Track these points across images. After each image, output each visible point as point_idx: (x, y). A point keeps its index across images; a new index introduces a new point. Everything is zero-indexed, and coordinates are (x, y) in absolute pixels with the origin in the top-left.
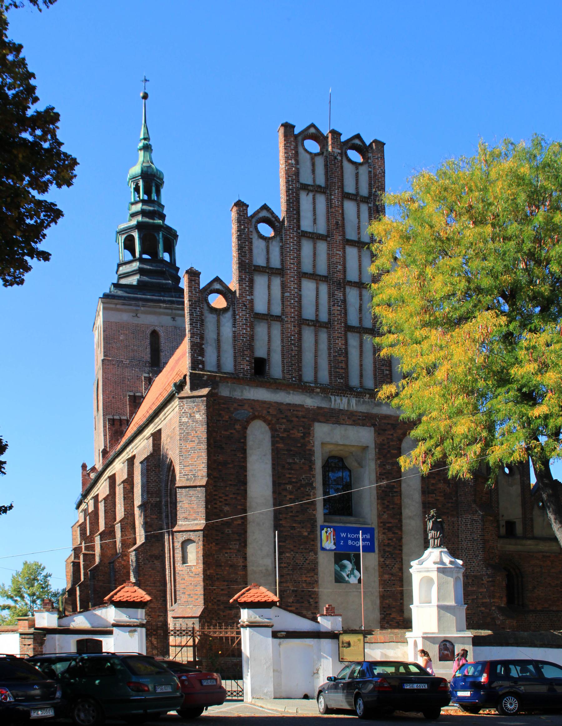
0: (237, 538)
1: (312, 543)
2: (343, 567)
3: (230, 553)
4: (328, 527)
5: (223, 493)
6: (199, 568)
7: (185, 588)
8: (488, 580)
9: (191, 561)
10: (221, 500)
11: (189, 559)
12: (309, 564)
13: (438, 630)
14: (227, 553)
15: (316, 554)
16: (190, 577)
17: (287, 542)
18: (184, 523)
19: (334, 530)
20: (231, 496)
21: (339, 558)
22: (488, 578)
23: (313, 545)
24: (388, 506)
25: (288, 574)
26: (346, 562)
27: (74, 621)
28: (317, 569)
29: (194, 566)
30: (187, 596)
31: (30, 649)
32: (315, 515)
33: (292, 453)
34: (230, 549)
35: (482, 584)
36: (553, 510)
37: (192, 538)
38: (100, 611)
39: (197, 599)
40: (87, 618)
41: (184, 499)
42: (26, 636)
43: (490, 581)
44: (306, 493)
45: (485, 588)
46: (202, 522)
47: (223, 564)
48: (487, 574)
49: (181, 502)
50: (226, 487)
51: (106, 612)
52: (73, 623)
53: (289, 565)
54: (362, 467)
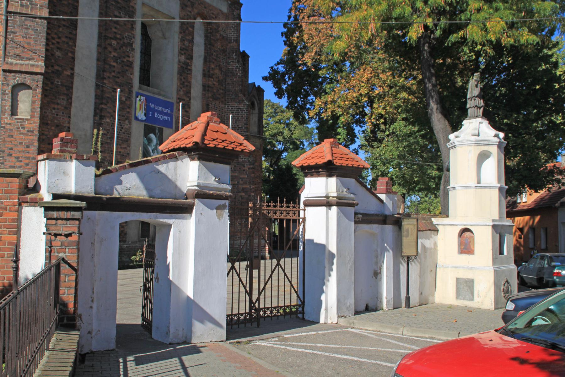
0: (65, 92)
1: (128, 110)
2: (150, 141)
3: (58, 109)
4: (142, 95)
5: (56, 34)
6: (34, 123)
7: (12, 149)
8: (249, 167)
9: (22, 112)
10: (54, 41)
11: (19, 111)
12: (124, 133)
13: (499, 218)
14: (54, 109)
15: (130, 123)
16: (21, 133)
17: (108, 105)
18: (15, 62)
19: (146, 100)
20: (64, 39)
21: (148, 130)
22: (250, 165)
23: (129, 112)
24: (184, 82)
25: (107, 142)
26: (152, 136)
27: (120, 183)
28: (130, 140)
29: (27, 119)
30: (14, 160)
31: (70, 244)
32: (132, 79)
33: (119, 5)
34: (58, 104)
35: (244, 170)
36: (436, 101)
37: (28, 82)
38: (165, 165)
39: (27, 165)
40: (142, 178)
41: (17, 30)
42: (62, 214)
43: (252, 168)
44: (127, 54)
45: (246, 174)
46: (40, 63)
47: (49, 122)
48: (249, 161)
49: (12, 32)
50: (59, 26)
51: (176, 168)
52: (118, 187)
53: (108, 133)
54: (165, 39)
